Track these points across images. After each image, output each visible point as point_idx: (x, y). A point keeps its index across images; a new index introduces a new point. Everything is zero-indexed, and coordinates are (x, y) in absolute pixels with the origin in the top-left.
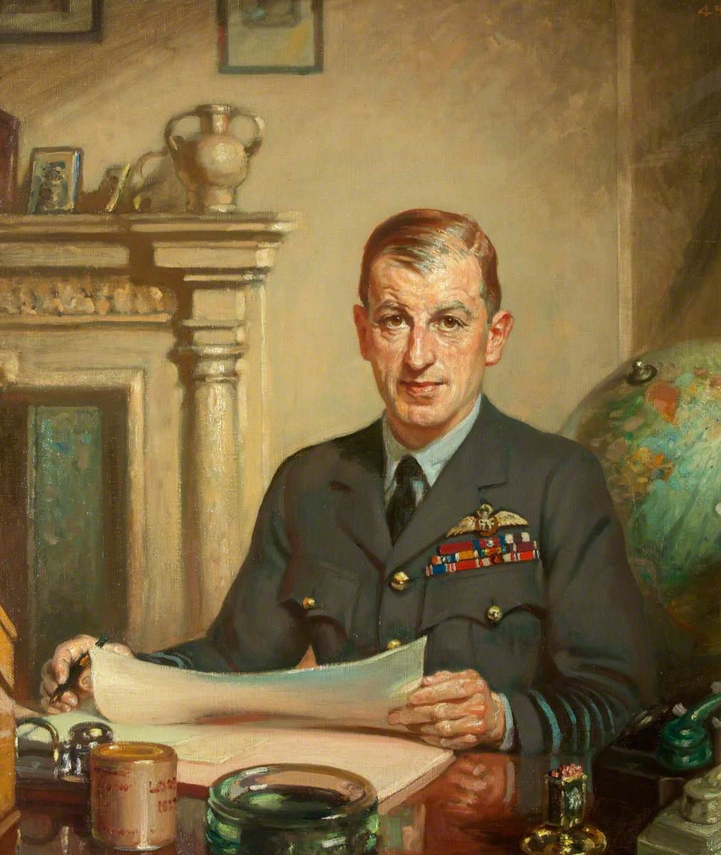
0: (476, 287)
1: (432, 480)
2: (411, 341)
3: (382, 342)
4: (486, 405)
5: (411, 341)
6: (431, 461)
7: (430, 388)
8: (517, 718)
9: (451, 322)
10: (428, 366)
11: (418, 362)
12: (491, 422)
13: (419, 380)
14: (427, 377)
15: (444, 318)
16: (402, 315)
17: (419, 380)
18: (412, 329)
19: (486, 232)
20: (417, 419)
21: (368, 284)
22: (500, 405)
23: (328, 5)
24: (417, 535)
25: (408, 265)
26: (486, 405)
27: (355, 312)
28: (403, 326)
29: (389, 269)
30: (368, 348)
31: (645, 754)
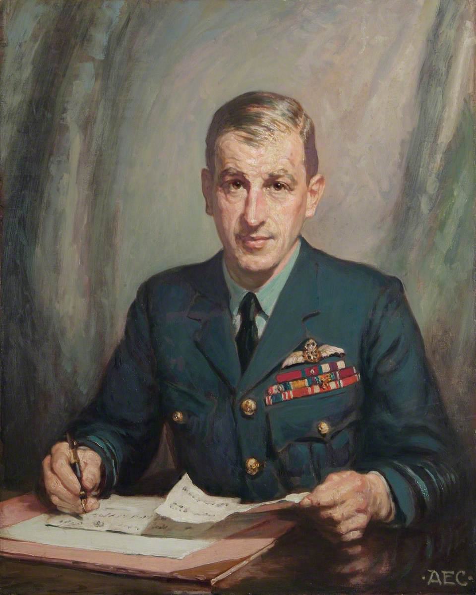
0: (300, 155)
1: (269, 312)
2: (247, 203)
3: (223, 202)
4: (305, 245)
5: (247, 203)
6: (268, 297)
7: (261, 242)
8: (391, 483)
9: (278, 186)
10: (262, 223)
11: (253, 221)
12: (311, 259)
13: (254, 235)
14: (262, 233)
15: (273, 183)
16: (240, 181)
17: (254, 235)
18: (248, 192)
19: (309, 114)
20: (254, 267)
21: (213, 152)
22: (315, 244)
23: (3, 535)
24: (260, 363)
25: (249, 141)
26: (305, 245)
27: (203, 175)
28: (242, 191)
29: (233, 143)
30: (213, 209)
31: (272, 504)
